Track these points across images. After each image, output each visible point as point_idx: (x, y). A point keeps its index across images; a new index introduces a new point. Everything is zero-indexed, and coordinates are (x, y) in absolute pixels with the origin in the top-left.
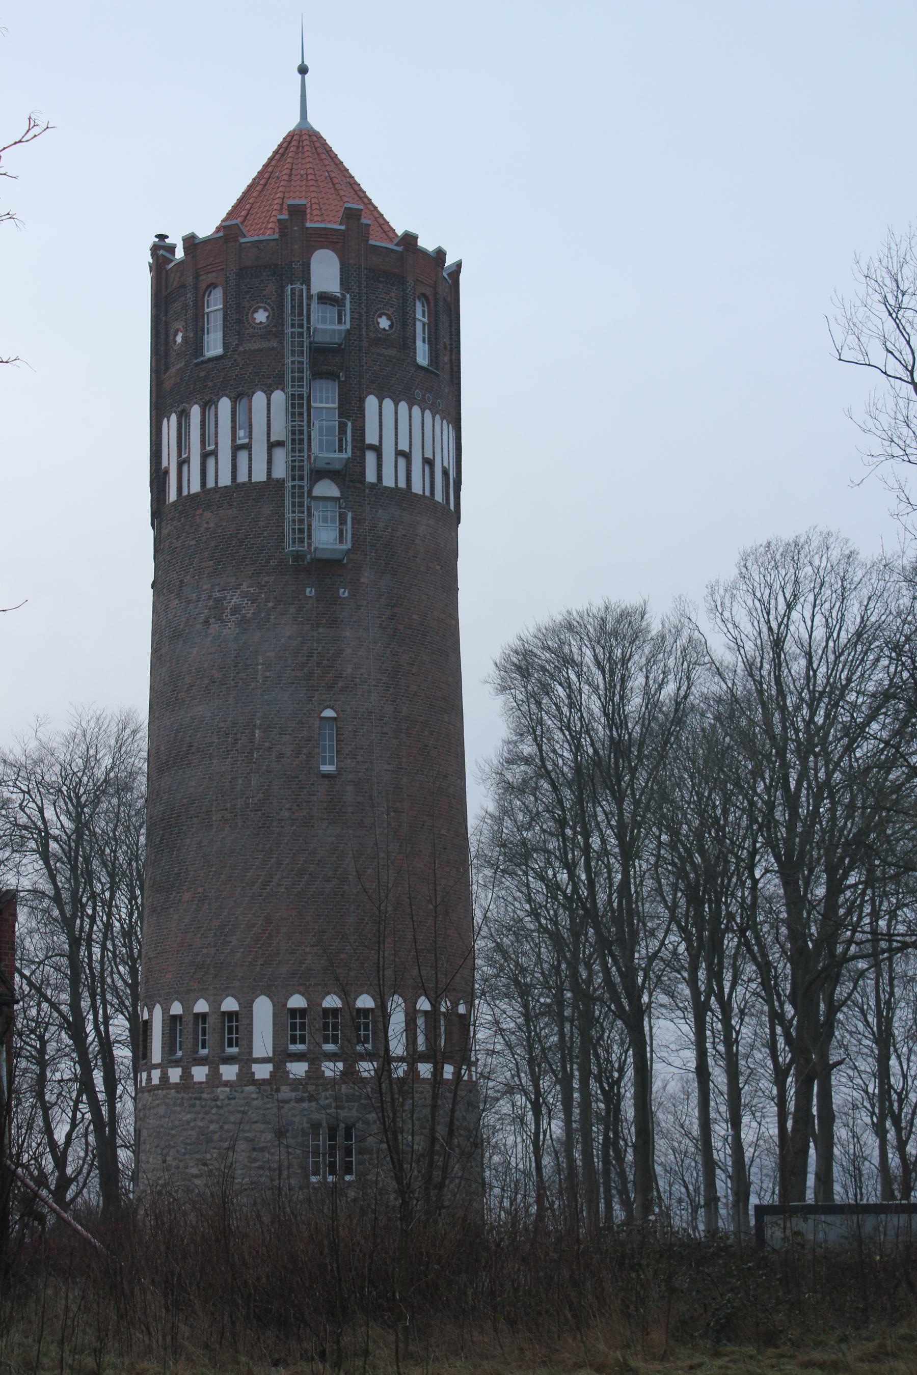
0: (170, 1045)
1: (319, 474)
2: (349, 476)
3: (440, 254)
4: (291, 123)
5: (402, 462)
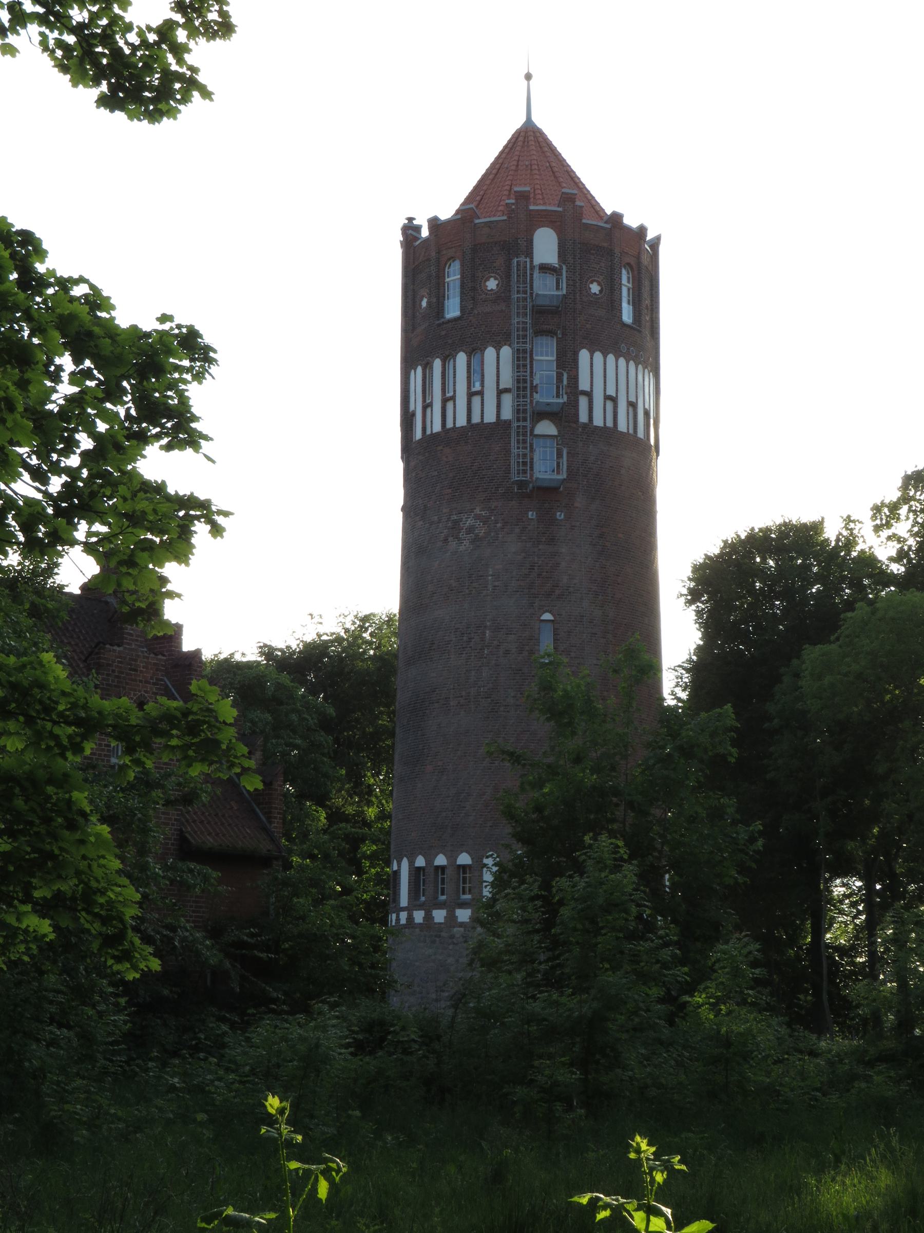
1: (540, 415)
2: (564, 416)
3: (642, 230)
4: (518, 122)
5: (610, 405)
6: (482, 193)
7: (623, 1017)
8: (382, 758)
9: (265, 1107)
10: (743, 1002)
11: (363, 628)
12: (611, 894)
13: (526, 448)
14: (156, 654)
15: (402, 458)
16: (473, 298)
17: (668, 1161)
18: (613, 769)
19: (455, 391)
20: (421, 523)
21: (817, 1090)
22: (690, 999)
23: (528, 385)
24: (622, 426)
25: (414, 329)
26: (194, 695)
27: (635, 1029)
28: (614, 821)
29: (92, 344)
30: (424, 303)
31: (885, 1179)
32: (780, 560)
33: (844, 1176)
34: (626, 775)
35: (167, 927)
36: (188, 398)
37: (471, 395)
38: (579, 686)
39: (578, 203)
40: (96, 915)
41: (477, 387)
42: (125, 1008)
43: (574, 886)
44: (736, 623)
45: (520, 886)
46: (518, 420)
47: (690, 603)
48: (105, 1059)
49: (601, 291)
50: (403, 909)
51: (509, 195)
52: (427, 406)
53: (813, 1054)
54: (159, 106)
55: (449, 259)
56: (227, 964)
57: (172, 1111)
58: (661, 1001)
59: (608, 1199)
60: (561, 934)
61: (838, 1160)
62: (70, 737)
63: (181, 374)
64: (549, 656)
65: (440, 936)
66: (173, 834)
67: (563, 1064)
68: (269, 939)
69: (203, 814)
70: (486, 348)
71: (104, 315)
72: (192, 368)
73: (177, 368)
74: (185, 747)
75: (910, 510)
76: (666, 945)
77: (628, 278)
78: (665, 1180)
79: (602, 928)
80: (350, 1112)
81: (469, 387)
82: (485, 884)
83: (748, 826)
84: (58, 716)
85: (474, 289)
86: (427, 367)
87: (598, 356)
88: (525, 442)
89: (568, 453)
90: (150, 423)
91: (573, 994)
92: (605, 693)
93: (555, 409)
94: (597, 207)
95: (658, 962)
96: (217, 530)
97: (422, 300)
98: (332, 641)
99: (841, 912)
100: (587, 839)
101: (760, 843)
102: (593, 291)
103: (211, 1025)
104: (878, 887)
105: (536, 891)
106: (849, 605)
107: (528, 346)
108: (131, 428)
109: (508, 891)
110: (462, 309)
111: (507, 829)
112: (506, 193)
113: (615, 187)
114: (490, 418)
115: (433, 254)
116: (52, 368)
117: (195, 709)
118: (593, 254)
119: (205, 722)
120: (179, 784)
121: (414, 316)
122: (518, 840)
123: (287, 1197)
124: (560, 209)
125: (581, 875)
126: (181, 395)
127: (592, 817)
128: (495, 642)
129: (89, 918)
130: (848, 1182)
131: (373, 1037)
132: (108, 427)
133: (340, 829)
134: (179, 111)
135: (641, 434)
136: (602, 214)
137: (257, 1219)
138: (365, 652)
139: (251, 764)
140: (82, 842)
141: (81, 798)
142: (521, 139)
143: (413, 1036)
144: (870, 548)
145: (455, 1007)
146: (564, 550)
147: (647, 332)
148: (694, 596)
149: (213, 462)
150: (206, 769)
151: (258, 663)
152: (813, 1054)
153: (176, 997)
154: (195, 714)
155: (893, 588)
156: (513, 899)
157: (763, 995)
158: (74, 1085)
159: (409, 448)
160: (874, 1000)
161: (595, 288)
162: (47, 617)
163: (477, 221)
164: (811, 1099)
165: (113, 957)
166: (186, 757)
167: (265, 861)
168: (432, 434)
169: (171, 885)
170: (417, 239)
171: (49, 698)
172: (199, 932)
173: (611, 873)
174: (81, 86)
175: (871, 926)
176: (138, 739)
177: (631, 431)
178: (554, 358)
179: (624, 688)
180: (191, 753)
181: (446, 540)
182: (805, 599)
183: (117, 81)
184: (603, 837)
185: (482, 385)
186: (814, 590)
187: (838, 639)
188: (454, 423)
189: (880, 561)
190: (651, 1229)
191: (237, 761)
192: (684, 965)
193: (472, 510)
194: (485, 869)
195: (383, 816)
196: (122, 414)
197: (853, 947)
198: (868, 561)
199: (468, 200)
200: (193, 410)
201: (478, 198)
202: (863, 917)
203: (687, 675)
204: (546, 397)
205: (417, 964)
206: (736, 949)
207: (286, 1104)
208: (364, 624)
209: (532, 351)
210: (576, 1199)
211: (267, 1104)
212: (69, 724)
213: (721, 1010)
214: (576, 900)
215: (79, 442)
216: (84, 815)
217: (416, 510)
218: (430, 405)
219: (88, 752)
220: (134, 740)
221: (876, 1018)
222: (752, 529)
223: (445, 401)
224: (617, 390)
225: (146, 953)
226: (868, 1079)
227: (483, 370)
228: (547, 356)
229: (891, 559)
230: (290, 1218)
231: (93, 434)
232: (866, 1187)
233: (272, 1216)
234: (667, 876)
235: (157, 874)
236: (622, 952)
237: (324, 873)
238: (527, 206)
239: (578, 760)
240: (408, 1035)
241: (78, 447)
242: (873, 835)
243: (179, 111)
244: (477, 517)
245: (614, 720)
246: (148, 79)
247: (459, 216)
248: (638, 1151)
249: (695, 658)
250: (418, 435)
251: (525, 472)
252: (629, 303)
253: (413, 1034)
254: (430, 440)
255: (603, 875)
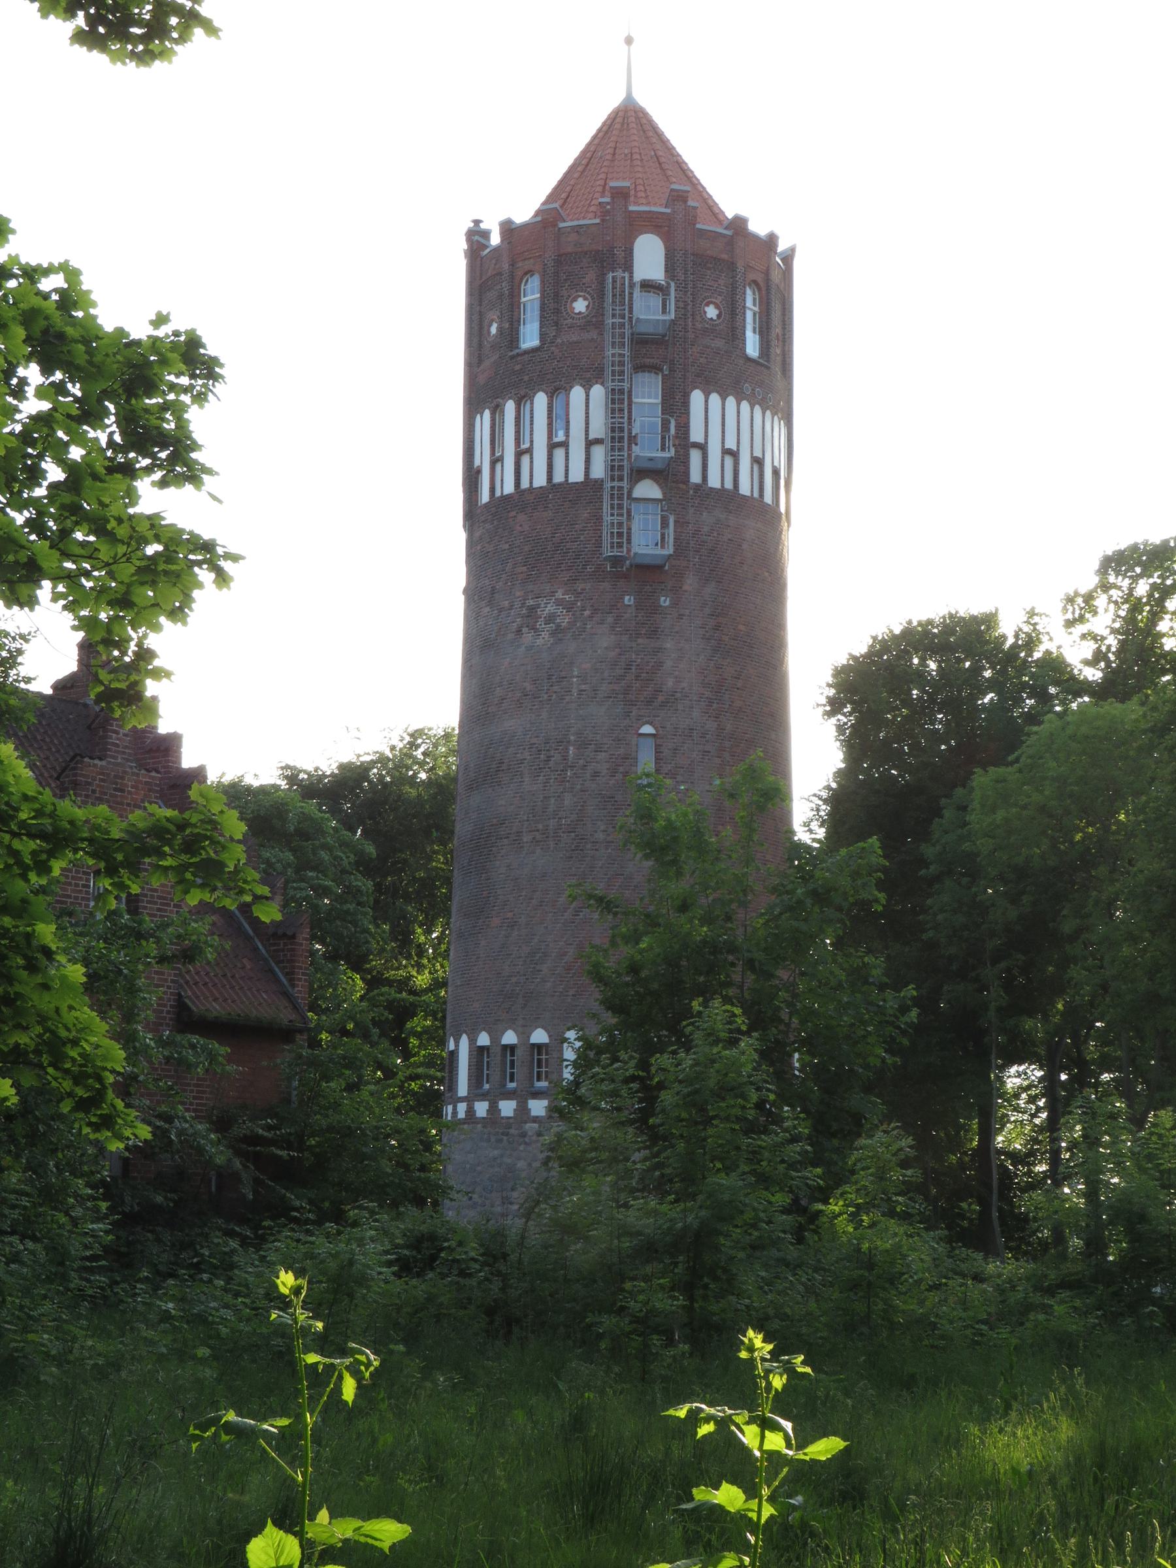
1: (640, 473)
2: (671, 475)
3: (772, 240)
5: (729, 461)
6: (568, 189)
7: (738, 1230)
8: (436, 909)
9: (277, 1287)
10: (891, 1213)
11: (413, 745)
12: (726, 1075)
13: (622, 515)
14: (148, 771)
15: (464, 526)
16: (556, 324)
17: (789, 1362)
18: (728, 918)
19: (532, 442)
20: (488, 609)
21: (983, 1322)
22: (823, 1208)
23: (626, 435)
24: (745, 489)
25: (480, 361)
26: (193, 802)
27: (753, 1247)
28: (728, 984)
29: (65, 349)
30: (494, 329)
31: (1066, 1430)
32: (943, 661)
33: (1015, 1426)
34: (745, 926)
35: (160, 1116)
36: (188, 421)
37: (552, 447)
38: (685, 815)
39: (691, 203)
40: (67, 1072)
41: (560, 437)
42: (106, 1216)
43: (677, 1066)
44: (887, 742)
45: (612, 1064)
46: (613, 479)
47: (829, 714)
48: (81, 1278)
49: (719, 316)
50: (462, 1100)
51: (603, 192)
52: (496, 460)
53: (978, 1278)
54: (151, 47)
55: (526, 274)
56: (237, 1164)
57: (165, 1346)
58: (786, 1211)
59: (712, 1411)
60: (662, 1125)
61: (1008, 1407)
62: (34, 853)
63: (177, 395)
64: (648, 775)
65: (507, 1134)
66: (169, 1000)
67: (662, 1287)
68: (290, 1134)
69: (207, 974)
70: (572, 387)
71: (80, 314)
72: (192, 387)
73: (173, 387)
74: (182, 868)
75: (1110, 600)
76: (794, 1140)
77: (754, 299)
78: (784, 1386)
79: (713, 1118)
80: (392, 1346)
81: (550, 437)
82: (566, 1063)
83: (899, 991)
84: (19, 828)
85: (557, 311)
86: (497, 410)
87: (715, 398)
88: (620, 507)
89: (675, 522)
90: (139, 453)
91: (676, 1201)
92: (720, 828)
93: (660, 466)
94: (715, 209)
95: (783, 1161)
96: (222, 578)
97: (490, 326)
98: (373, 762)
99: (1017, 1109)
100: (696, 1005)
101: (914, 1014)
102: (709, 316)
103: (216, 1241)
104: (1063, 1077)
105: (631, 1072)
106: (1032, 718)
107: (626, 385)
108: (115, 459)
109: (597, 1069)
110: (543, 337)
111: (592, 998)
112: (600, 189)
113: (736, 186)
114: (577, 475)
115: (506, 266)
116: (14, 381)
117: (193, 821)
118: (709, 269)
119: (206, 838)
120: (179, 937)
121: (480, 346)
122: (608, 1008)
123: (306, 1441)
124: (668, 211)
125: (688, 1051)
126: (182, 424)
127: (702, 979)
128: (581, 762)
129: (58, 1074)
130: (1019, 1433)
131: (421, 1255)
132: (84, 452)
133: (382, 995)
134: (175, 53)
135: (768, 498)
136: (721, 217)
137: (265, 1427)
138: (415, 775)
139: (264, 890)
140: (46, 987)
141: (46, 932)
142: (618, 120)
143: (473, 1254)
144: (1059, 647)
145: (528, 1215)
146: (668, 645)
147: (777, 369)
148: (835, 706)
149: (220, 501)
150: (207, 897)
151: (276, 787)
152: (978, 1278)
153: (171, 1205)
154: (194, 826)
155: (1086, 699)
156: (603, 1080)
157: (915, 1202)
158: (41, 1310)
159: (473, 514)
160: (1056, 1212)
161: (711, 312)
162: (8, 720)
163: (562, 225)
164: (974, 1334)
165: (90, 1124)
166: (182, 881)
167: (286, 1034)
168: (502, 496)
169: (166, 1063)
170: (486, 247)
171: (7, 804)
172: (201, 1123)
173: (725, 1048)
174: (52, 17)
175: (1052, 1125)
176: (120, 857)
177: (756, 495)
178: (659, 401)
179: (742, 817)
180: (188, 876)
181: (519, 631)
182: (976, 710)
183: (97, 9)
184: (717, 1002)
185: (567, 435)
186: (986, 701)
187: (1017, 760)
188: (531, 483)
189: (1070, 665)
190: (766, 1447)
191: (248, 887)
192: (815, 1165)
193: (553, 593)
194: (565, 1045)
195: (437, 984)
196: (103, 441)
197: (1032, 1153)
198: (1055, 667)
199: (551, 198)
200: (194, 435)
201: (564, 196)
202: (1044, 1115)
203: (824, 807)
204: (648, 450)
205: (479, 1168)
206: (883, 1144)
207: (303, 1282)
208: (416, 739)
209: (630, 392)
210: (671, 1412)
211: (278, 1282)
212: (32, 836)
213: (863, 1221)
214: (680, 1082)
215: (46, 471)
216: (48, 953)
217: (482, 594)
218: (500, 459)
219: (56, 872)
220: (115, 859)
221: (1059, 1238)
222: (910, 622)
223: (519, 454)
224: (738, 442)
225: (131, 1118)
226: (1047, 1309)
227: (568, 415)
228: (649, 397)
229: (1087, 663)
230: (307, 1426)
231: (62, 462)
232: (1042, 1440)
233: (284, 1422)
234: (796, 1055)
235: (148, 1046)
236: (738, 1148)
237: (361, 1050)
238: (626, 207)
239: (684, 907)
240: (466, 1253)
241: (45, 479)
242: (1058, 1011)
243: (175, 53)
244: (559, 603)
245: (730, 857)
246: (137, 11)
247: (539, 219)
248: (751, 1349)
249: (834, 785)
250: (485, 497)
251: (620, 545)
252: (754, 332)
253: (473, 1250)
254: (501, 504)
255: (715, 1050)
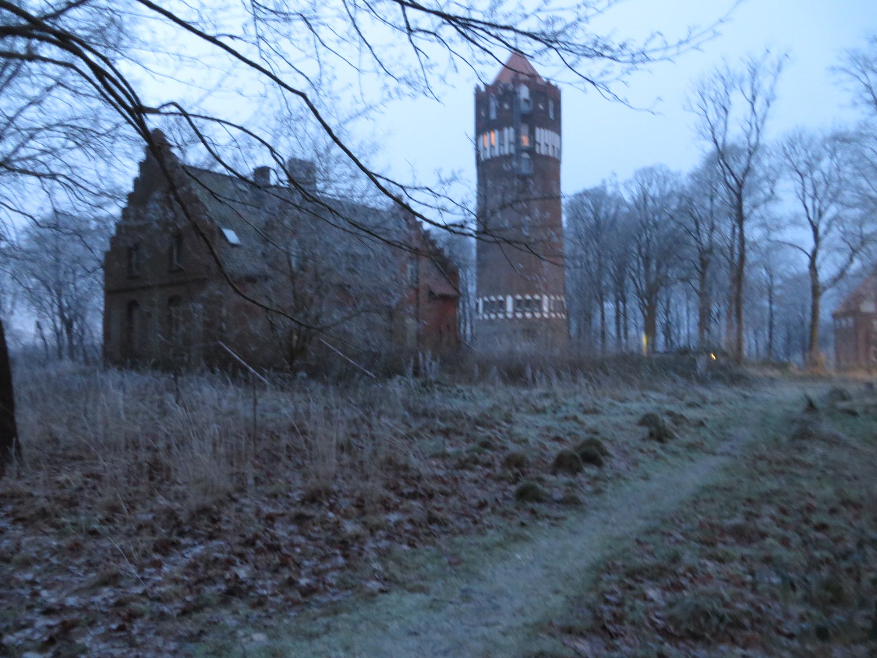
0: (484, 309)
1: (523, 151)
2: (531, 151)
